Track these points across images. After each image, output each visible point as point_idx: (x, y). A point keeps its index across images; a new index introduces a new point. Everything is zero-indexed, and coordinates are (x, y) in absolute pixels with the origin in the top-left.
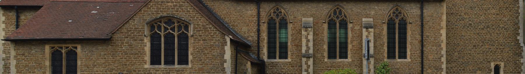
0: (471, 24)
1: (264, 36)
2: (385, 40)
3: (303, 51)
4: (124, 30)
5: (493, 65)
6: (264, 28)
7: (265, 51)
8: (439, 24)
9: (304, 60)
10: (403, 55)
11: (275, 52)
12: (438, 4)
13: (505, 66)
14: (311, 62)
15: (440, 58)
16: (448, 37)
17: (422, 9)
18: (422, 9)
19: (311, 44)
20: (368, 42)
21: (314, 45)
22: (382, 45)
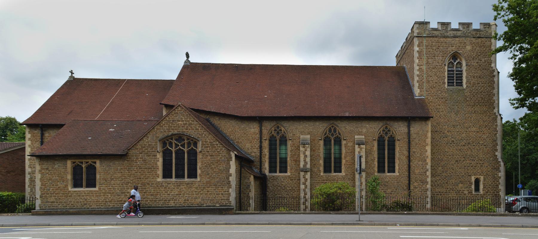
0: (453, 141)
2: (376, 155)
3: (302, 166)
6: (266, 144)
7: (267, 165)
8: (425, 141)
9: (302, 174)
10: (392, 169)
12: (423, 123)
13: (484, 180)
14: (308, 176)
15: (425, 172)
16: (433, 153)
21: (311, 160)
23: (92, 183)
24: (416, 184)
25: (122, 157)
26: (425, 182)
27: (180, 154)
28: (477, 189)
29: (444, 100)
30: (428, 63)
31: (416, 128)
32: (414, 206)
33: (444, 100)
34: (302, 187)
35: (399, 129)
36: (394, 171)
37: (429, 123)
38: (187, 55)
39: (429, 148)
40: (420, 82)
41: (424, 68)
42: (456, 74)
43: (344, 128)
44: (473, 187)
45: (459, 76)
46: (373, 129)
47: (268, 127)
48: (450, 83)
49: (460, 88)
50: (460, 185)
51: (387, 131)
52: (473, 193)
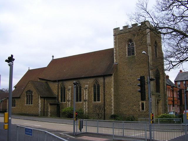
0: (131, 84)
1: (60, 94)
2: (93, 94)
3: (85, 99)
4: (106, 83)
5: (140, 103)
6: (60, 90)
7: (60, 99)
8: (111, 86)
9: (68, 102)
10: (99, 100)
11: (96, 100)
12: (110, 77)
13: (146, 103)
14: (87, 103)
15: (111, 101)
16: (115, 91)
17: (104, 79)
18: (104, 79)
19: (70, 96)
20: (86, 95)
21: (71, 96)
22: (92, 96)
23: (15, 106)
24: (107, 106)
25: (19, 98)
26: (111, 106)
27: (168, 88)
28: (143, 109)
29: (126, 63)
30: (119, 46)
31: (107, 80)
32: (136, 116)
33: (126, 63)
34: (84, 106)
35: (101, 80)
36: (99, 100)
37: (113, 77)
38: (53, 57)
39: (112, 89)
40: (116, 56)
41: (117, 49)
42: (132, 49)
43: (82, 82)
44: (141, 107)
45: (133, 50)
46: (91, 81)
47: (60, 83)
48: (129, 54)
49: (133, 56)
50: (135, 107)
51: (97, 82)
52: (141, 111)
